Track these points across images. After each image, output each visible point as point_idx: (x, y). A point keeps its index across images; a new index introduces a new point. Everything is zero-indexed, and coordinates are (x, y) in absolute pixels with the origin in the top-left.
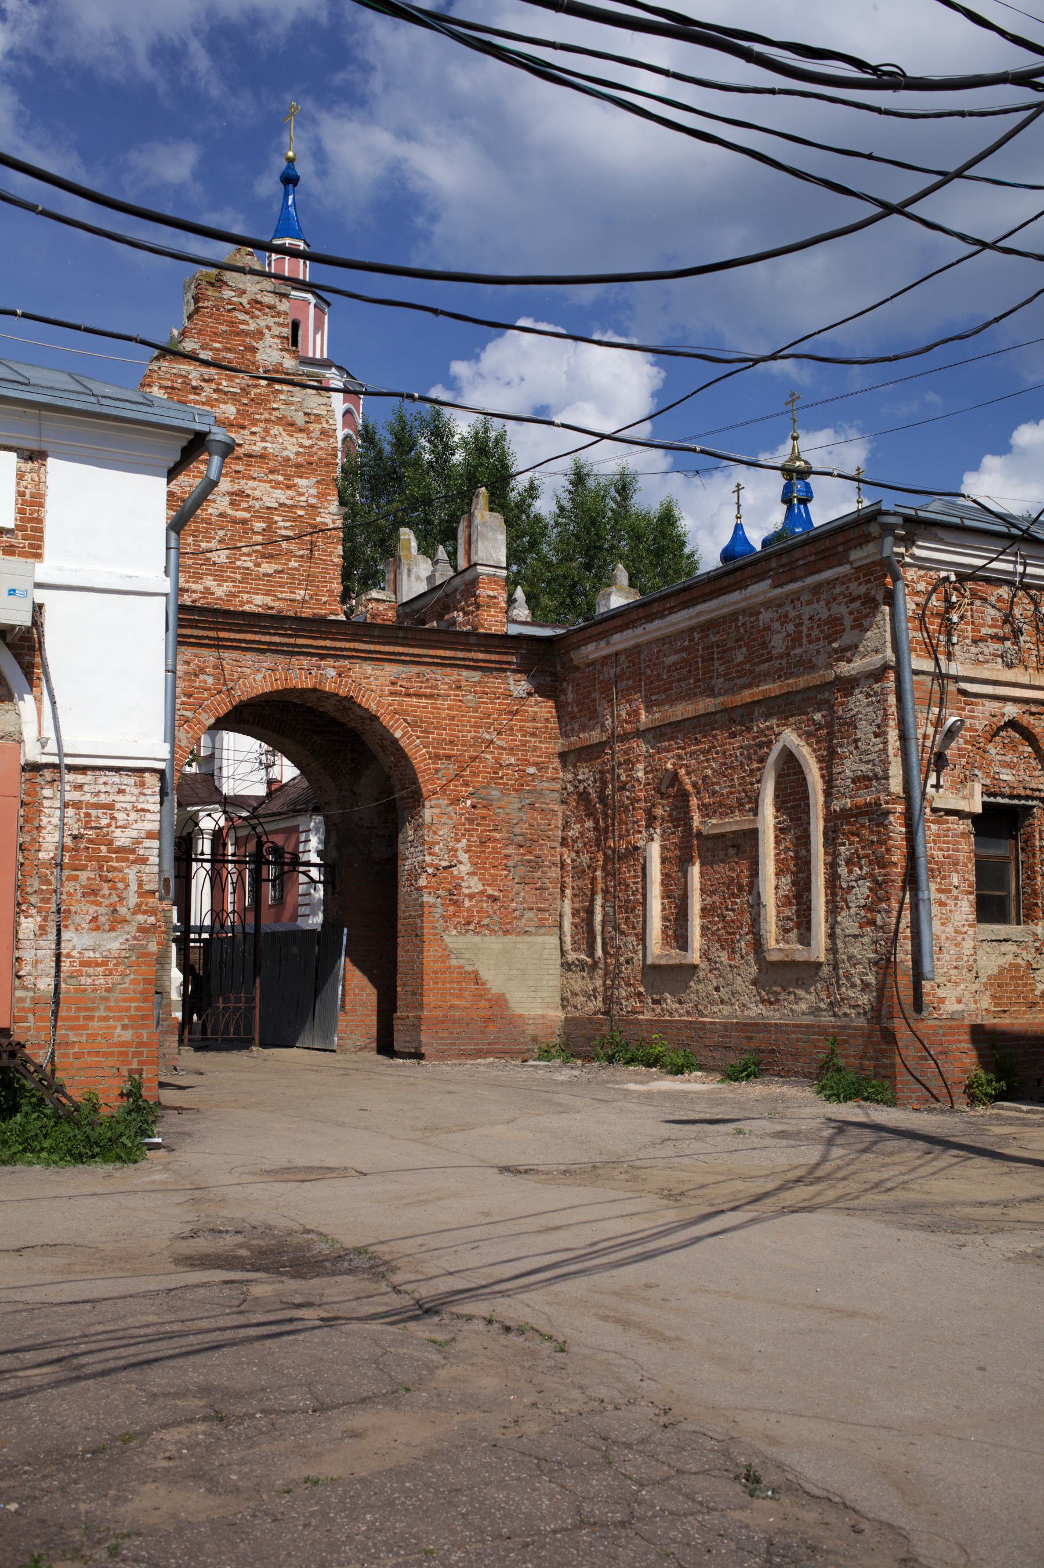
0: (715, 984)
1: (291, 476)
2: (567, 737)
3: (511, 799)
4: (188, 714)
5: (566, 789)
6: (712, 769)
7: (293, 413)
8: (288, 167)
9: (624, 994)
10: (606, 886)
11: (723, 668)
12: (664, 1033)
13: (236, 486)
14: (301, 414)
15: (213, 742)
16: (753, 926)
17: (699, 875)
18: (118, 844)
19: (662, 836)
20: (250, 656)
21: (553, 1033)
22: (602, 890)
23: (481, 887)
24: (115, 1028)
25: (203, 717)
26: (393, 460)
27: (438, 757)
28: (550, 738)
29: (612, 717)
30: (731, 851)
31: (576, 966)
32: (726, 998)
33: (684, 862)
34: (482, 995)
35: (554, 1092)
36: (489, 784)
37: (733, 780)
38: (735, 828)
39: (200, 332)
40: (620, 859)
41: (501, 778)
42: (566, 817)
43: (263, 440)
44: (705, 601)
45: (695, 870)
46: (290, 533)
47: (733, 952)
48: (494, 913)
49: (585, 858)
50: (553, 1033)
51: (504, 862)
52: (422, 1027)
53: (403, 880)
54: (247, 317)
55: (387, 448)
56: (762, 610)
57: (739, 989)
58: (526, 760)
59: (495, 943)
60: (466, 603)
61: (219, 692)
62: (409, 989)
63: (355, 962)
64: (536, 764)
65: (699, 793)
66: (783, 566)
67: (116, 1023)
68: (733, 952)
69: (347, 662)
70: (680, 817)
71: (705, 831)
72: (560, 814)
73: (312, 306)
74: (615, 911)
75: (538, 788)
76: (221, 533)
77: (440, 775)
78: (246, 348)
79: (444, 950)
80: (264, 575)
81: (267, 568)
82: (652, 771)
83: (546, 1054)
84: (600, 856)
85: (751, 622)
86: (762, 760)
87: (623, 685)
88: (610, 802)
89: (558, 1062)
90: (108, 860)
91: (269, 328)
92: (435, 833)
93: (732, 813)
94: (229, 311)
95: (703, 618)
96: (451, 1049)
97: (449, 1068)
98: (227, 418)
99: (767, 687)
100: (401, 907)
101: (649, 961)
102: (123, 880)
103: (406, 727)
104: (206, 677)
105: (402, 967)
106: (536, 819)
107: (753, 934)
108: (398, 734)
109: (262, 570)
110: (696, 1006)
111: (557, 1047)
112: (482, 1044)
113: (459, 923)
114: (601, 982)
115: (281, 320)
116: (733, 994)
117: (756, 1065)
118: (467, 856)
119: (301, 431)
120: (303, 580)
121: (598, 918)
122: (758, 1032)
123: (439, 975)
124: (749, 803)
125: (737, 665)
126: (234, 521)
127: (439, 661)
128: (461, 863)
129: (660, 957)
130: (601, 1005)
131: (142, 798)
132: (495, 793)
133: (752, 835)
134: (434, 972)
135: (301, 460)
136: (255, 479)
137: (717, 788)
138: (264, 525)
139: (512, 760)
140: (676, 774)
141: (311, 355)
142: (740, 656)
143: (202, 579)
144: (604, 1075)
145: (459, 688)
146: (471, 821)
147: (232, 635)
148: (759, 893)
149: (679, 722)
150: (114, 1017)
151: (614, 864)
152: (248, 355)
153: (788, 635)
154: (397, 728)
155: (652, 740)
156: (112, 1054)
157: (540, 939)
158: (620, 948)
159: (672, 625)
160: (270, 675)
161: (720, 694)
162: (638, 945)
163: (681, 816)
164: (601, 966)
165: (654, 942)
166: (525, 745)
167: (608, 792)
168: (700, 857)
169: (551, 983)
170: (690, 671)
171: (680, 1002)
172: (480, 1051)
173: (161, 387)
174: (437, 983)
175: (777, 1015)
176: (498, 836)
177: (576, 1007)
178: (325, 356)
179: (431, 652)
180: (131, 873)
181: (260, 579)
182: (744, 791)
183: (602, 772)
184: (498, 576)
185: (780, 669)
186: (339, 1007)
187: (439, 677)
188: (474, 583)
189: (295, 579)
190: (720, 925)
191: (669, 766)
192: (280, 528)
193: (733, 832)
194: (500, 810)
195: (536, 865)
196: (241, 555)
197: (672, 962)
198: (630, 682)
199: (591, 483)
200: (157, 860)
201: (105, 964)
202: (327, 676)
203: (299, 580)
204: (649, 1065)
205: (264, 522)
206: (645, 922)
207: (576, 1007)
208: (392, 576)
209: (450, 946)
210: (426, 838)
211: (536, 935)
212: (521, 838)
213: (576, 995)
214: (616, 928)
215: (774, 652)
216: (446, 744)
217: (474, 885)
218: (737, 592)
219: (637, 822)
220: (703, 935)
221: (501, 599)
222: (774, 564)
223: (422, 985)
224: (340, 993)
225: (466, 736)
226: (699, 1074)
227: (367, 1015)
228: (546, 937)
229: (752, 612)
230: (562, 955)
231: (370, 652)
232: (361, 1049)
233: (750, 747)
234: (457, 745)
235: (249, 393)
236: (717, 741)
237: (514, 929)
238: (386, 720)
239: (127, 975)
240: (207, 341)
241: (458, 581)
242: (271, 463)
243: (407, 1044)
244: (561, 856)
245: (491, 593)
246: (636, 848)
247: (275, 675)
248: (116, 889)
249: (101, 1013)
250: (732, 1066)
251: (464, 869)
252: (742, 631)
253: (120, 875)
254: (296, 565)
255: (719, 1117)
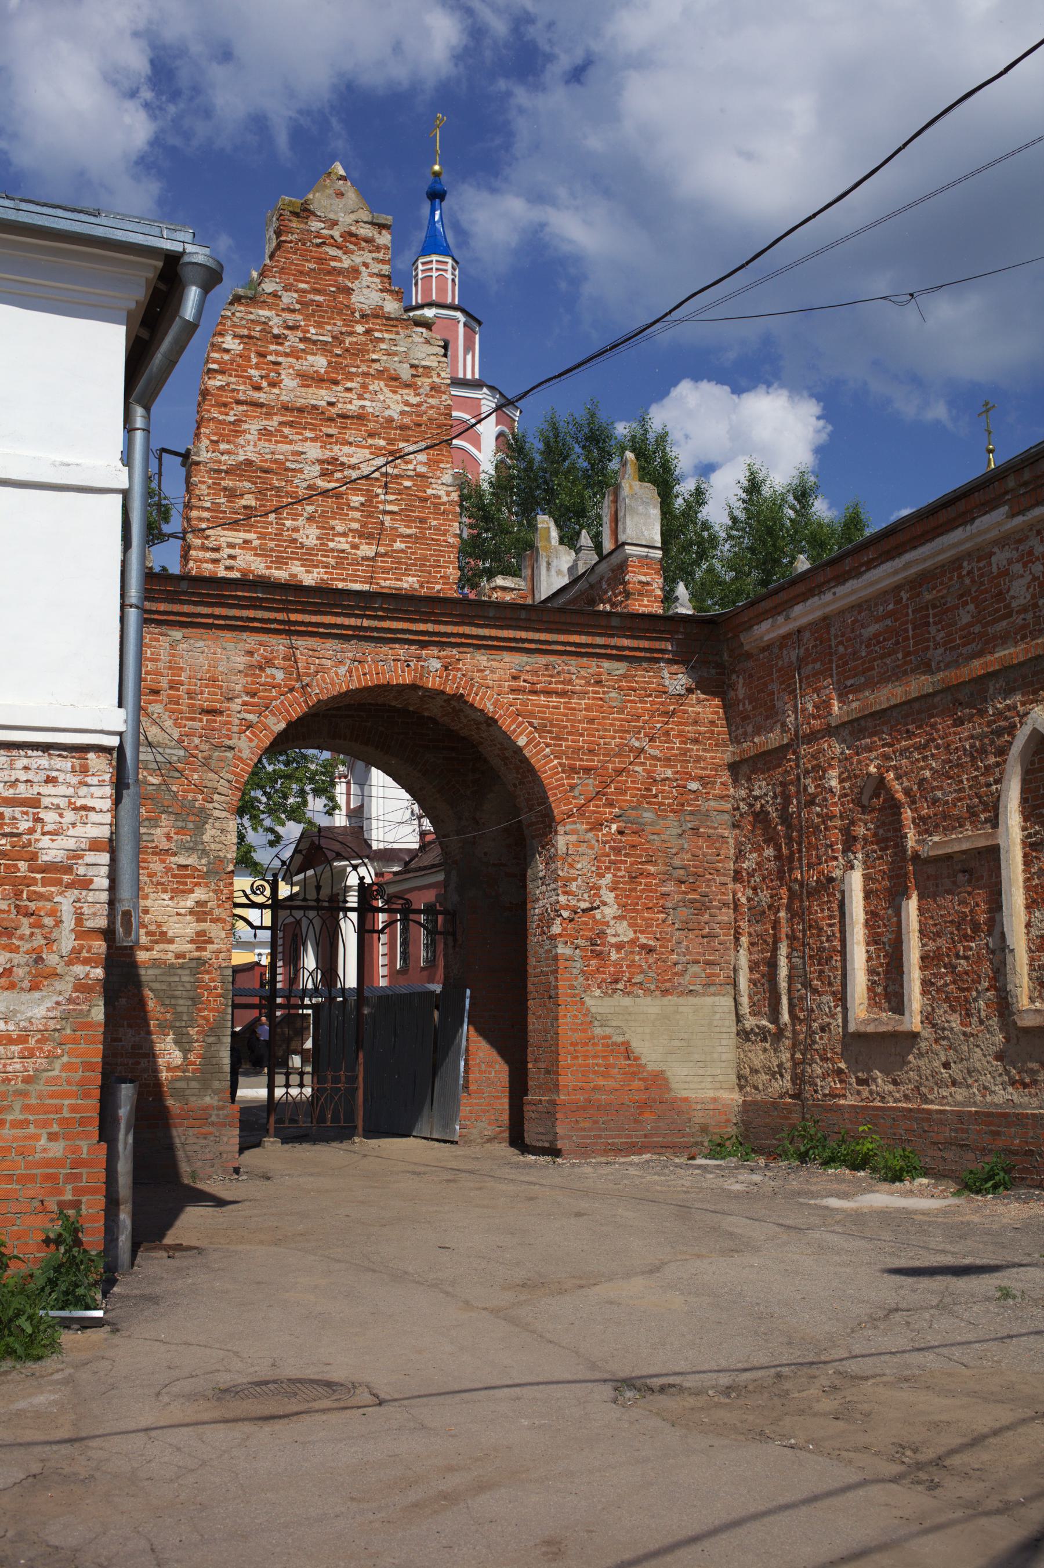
0: (943, 1059)
1: (395, 440)
2: (739, 743)
3: (668, 823)
4: (251, 717)
5: (738, 808)
6: (931, 769)
7: (397, 365)
8: (435, 182)
9: (819, 1071)
10: (793, 931)
11: (942, 634)
12: (874, 1125)
13: (328, 452)
14: (406, 366)
15: (362, 791)
16: (995, 979)
17: (916, 912)
18: (45, 858)
19: (865, 862)
20: (330, 644)
21: (728, 1121)
22: (787, 936)
23: (631, 935)
24: (38, 1138)
25: (271, 721)
26: (545, 471)
27: (573, 770)
28: (716, 745)
29: (796, 712)
30: (961, 878)
31: (756, 1034)
32: (959, 1078)
33: (896, 895)
34: (634, 1073)
35: (724, 1213)
36: (640, 803)
37: (961, 782)
38: (965, 846)
39: (282, 271)
40: (810, 894)
41: (656, 796)
42: (739, 845)
43: (361, 397)
44: (915, 547)
45: (912, 905)
46: (395, 508)
47: (969, 1015)
48: (650, 967)
49: (764, 896)
50: (728, 1121)
51: (661, 902)
52: (558, 1116)
53: (533, 927)
54: (339, 253)
55: (538, 457)
56: (996, 550)
57: (978, 1065)
58: (687, 773)
59: (650, 1006)
60: (614, 593)
61: (292, 690)
62: (542, 1065)
63: (482, 1032)
64: (700, 778)
65: (914, 802)
66: (1025, 484)
67: (39, 1131)
68: (969, 1015)
69: (455, 652)
70: (889, 835)
71: (924, 852)
72: (731, 841)
73: (461, 325)
74: (804, 963)
75: (703, 809)
76: (310, 509)
77: (576, 793)
78: (338, 288)
79: (585, 1015)
80: (362, 558)
81: (367, 550)
82: (849, 778)
83: (718, 1150)
84: (784, 892)
85: (979, 569)
86: (1002, 752)
87: (808, 670)
88: (795, 822)
89: (733, 1161)
90: (30, 882)
91: (366, 265)
92: (571, 866)
93: (960, 826)
94: (318, 245)
95: (913, 570)
96: (595, 1144)
97: (592, 1171)
98: (317, 372)
99: (1006, 652)
100: (532, 961)
101: (852, 1028)
102: (53, 913)
103: (531, 733)
104: (274, 671)
105: (533, 1038)
106: (701, 848)
107: (996, 989)
108: (522, 742)
109: (360, 553)
110: (917, 1088)
111: (734, 1139)
112: (636, 1136)
113: (604, 981)
114: (788, 1055)
115: (381, 256)
116: (969, 1072)
117: (1007, 1171)
118: (613, 895)
119: (407, 386)
120: (412, 565)
121: (783, 972)
122: (1009, 1125)
123: (579, 1048)
124: (984, 811)
125: (962, 629)
126: (325, 493)
127: (573, 649)
128: (605, 904)
129: (867, 1022)
130: (789, 1085)
131: (83, 791)
132: (648, 815)
133: (992, 854)
134: (572, 1044)
135: (407, 420)
136: (351, 444)
137: (939, 794)
138: (363, 499)
139: (669, 773)
140: (881, 779)
141: (461, 375)
142: (965, 617)
143: (287, 564)
144: (795, 1183)
145: (598, 683)
146: (617, 851)
147: (307, 618)
148: (1003, 934)
149: (885, 710)
150: (36, 1120)
151: (801, 901)
152: (341, 298)
153: (1035, 578)
154: (521, 734)
155: (848, 738)
156: (31, 1178)
157: (709, 1000)
158: (812, 1010)
159: (872, 584)
160: (357, 669)
161: (939, 669)
162: (836, 1007)
163: (890, 834)
164: (788, 1034)
165: (857, 1002)
166: (685, 755)
167: (792, 809)
168: (917, 888)
169: (724, 1057)
170: (897, 643)
171: (895, 1083)
172: (634, 1145)
173: (235, 336)
174: (576, 1058)
175: (1035, 1102)
176: (652, 869)
177: (756, 1088)
178: (477, 376)
179: (562, 638)
180: (66, 903)
181: (358, 564)
182: (978, 795)
183: (783, 784)
184: (652, 558)
185: (1024, 627)
186: (460, 1087)
187: (573, 669)
188: (622, 567)
189: (401, 563)
190: (948, 979)
191: (872, 769)
192: (383, 502)
193: (963, 852)
194: (655, 837)
195: (702, 906)
196: (334, 535)
197: (882, 1029)
198: (818, 666)
199: (766, 492)
200: (105, 883)
201: (22, 1040)
202: (431, 669)
203: (406, 564)
204: (855, 1167)
205: (363, 495)
206: (844, 976)
207: (756, 1088)
208: (529, 572)
209: (593, 1010)
210: (560, 873)
211: (703, 995)
212: (682, 872)
213: (757, 1072)
214: (807, 984)
215: (1014, 604)
216: (584, 754)
217: (622, 932)
218: (961, 529)
219: (831, 846)
220: (924, 993)
221: (655, 585)
222: (1011, 483)
223: (557, 1060)
224: (462, 1069)
225: (609, 744)
226: (925, 1181)
227: (497, 1098)
228: (717, 998)
229: (982, 554)
230: (738, 1021)
231: (484, 638)
232: (489, 1141)
233: (981, 737)
234: (598, 755)
235: (343, 342)
236: (937, 731)
237: (675, 988)
238: (507, 724)
239: (58, 1057)
240: (291, 281)
241: (603, 566)
242: (371, 425)
243: (540, 1137)
244: (734, 894)
245: (643, 578)
246: (831, 880)
247: (363, 668)
248: (42, 927)
249: (16, 1115)
250: (971, 1172)
251: (610, 911)
252: (967, 581)
253: (49, 905)
254: (403, 546)
255: (968, 1261)
